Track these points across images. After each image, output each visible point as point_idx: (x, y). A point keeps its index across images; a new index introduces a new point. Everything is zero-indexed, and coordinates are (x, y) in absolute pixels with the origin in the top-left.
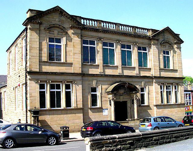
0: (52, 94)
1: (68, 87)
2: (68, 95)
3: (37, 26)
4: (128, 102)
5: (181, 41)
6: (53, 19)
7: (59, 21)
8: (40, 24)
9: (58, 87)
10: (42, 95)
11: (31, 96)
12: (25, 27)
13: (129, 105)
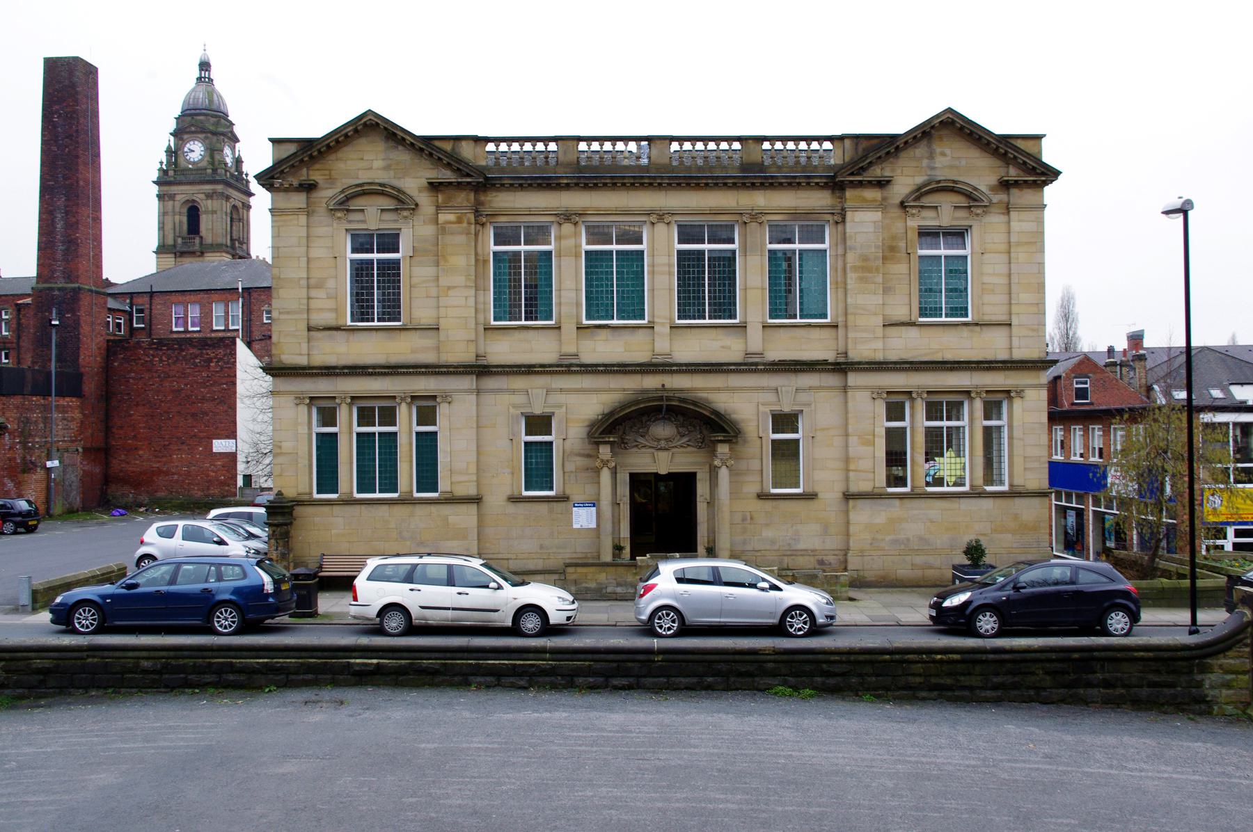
0: (364, 441)
1: (427, 416)
2: (427, 445)
3: (299, 200)
4: (699, 477)
5: (1043, 174)
6: (361, 164)
7: (387, 168)
8: (309, 188)
9: (389, 416)
10: (327, 445)
11: (279, 451)
12: (933, 131)
13: (702, 489)
